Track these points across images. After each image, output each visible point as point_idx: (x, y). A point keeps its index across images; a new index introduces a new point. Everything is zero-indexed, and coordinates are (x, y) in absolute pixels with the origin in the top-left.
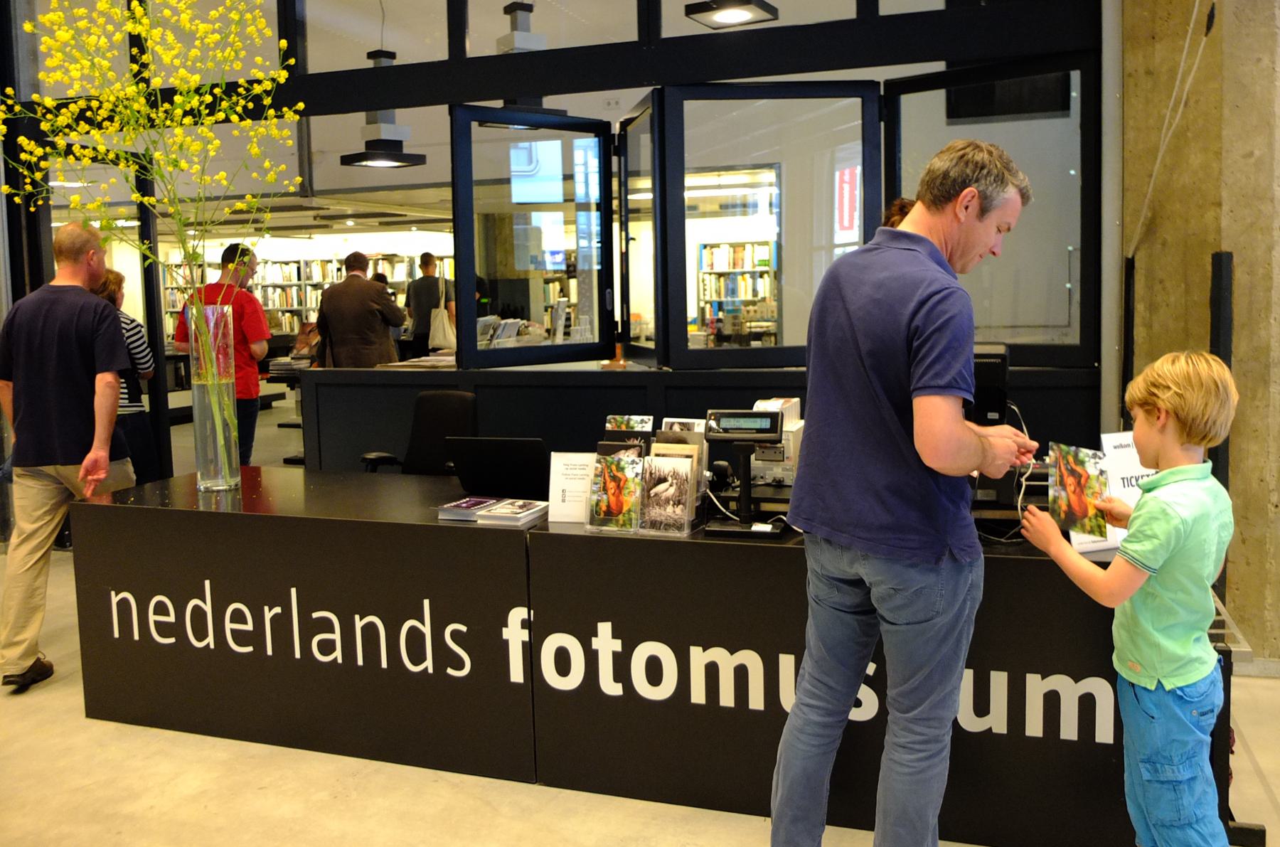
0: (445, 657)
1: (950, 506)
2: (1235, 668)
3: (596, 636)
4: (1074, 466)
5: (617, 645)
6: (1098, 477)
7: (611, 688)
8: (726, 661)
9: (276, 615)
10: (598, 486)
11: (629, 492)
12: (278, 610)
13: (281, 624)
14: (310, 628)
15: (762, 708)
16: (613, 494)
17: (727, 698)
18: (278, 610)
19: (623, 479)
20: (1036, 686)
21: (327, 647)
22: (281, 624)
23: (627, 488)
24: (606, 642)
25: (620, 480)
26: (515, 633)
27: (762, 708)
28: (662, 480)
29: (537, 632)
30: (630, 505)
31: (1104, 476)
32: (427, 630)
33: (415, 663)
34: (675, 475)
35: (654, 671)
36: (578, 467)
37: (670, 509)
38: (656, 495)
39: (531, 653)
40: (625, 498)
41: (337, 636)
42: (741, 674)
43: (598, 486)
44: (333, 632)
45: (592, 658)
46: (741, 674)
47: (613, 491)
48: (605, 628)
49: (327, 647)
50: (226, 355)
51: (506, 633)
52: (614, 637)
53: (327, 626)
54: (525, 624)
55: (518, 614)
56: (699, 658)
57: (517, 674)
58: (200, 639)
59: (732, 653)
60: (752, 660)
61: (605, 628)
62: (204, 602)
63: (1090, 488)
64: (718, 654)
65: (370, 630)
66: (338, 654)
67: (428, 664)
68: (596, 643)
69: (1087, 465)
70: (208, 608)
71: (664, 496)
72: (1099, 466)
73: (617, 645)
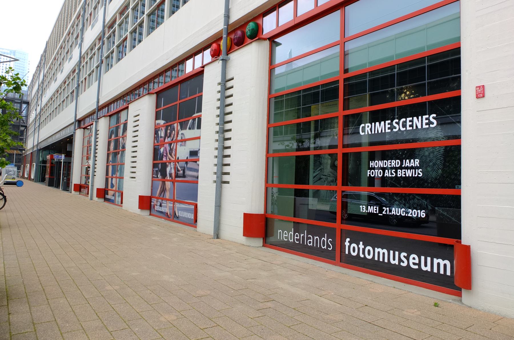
0: (328, 246)
1: (281, 147)
2: (172, 207)
3: (360, 244)
7: (362, 256)
8: (442, 262)
9: (303, 236)
12: (303, 235)
13: (303, 237)
14: (308, 238)
15: (450, 275)
17: (442, 272)
18: (303, 235)
20: (436, 261)
22: (303, 237)
24: (361, 246)
26: (347, 244)
27: (450, 275)
28: (11, 171)
29: (351, 242)
32: (326, 240)
33: (323, 247)
34: (13, 171)
36: (91, 162)
37: (12, 176)
38: (10, 174)
41: (312, 240)
42: (445, 266)
44: (311, 239)
46: (445, 266)
48: (361, 243)
50: (83, 9)
51: (346, 244)
52: (363, 245)
53: (310, 238)
54: (349, 242)
55: (348, 240)
56: (377, 250)
57: (347, 253)
58: (323, 247)
59: (443, 261)
60: (385, 251)
61: (361, 243)
62: (325, 238)
64: (440, 261)
65: (317, 239)
66: (311, 244)
67: (325, 247)
68: (360, 246)
70: (293, 234)
71: (11, 174)
73: (363, 247)
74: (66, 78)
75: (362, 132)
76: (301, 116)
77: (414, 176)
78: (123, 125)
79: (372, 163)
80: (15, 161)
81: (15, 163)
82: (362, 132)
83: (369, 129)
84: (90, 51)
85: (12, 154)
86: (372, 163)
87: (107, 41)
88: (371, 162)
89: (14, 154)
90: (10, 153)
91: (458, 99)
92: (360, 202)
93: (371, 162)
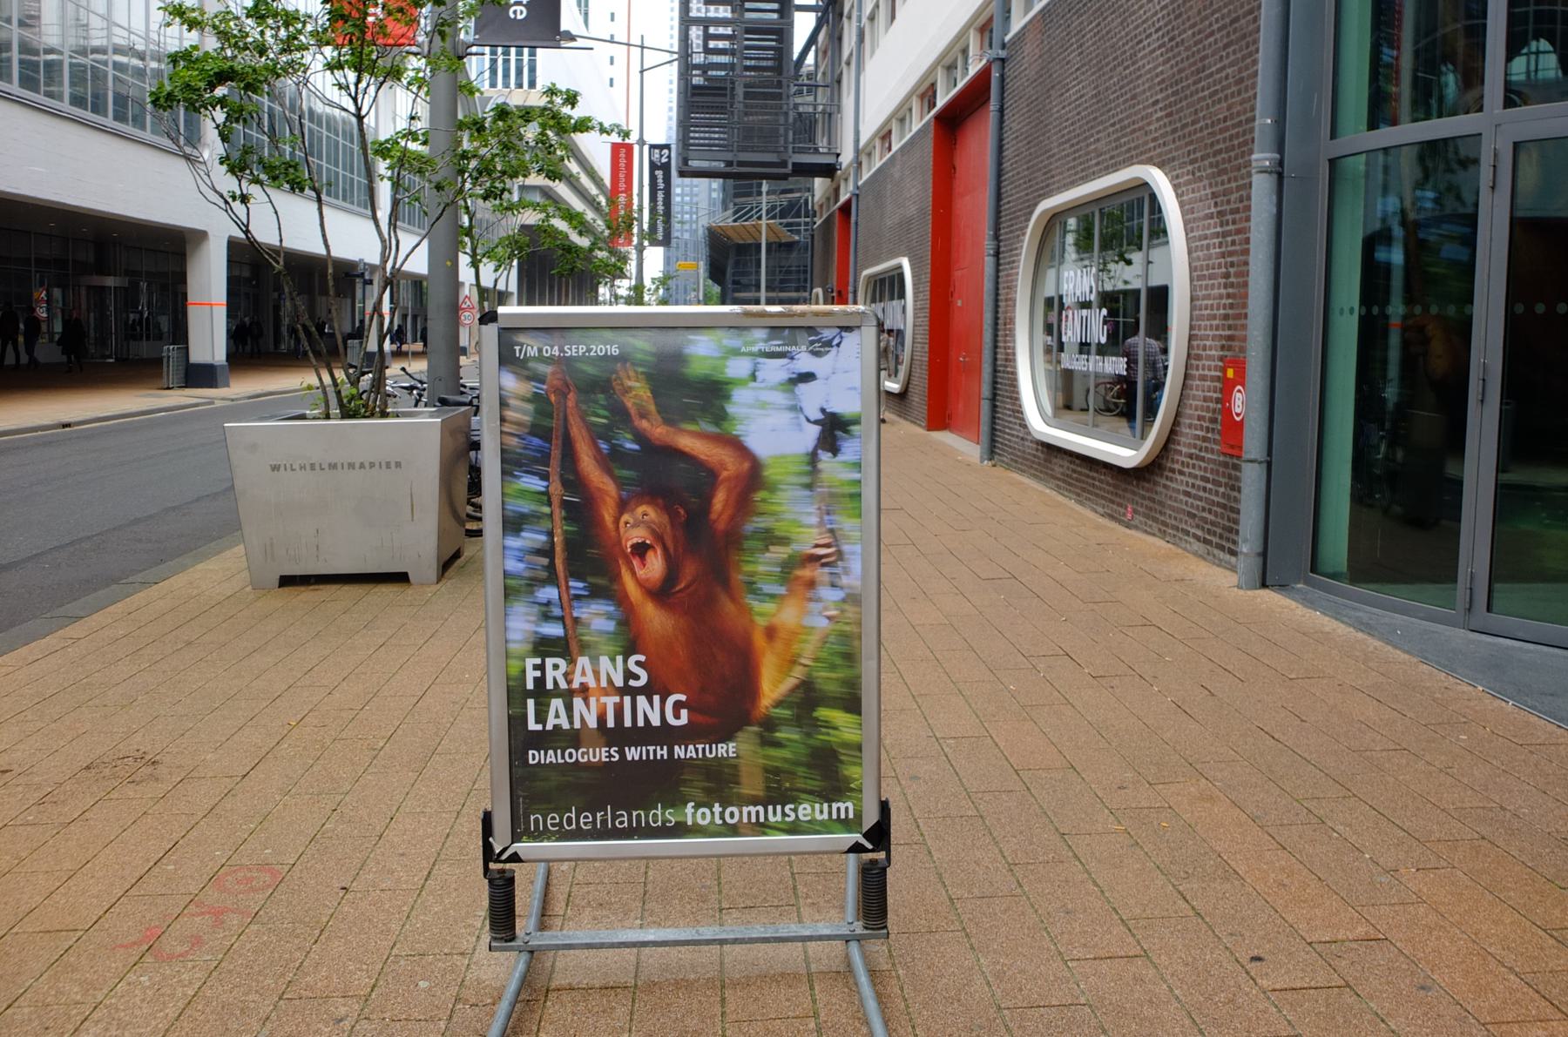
4: (658, 431)
5: (721, 809)
6: (813, 458)
10: (532, 538)
11: (788, 569)
16: (661, 593)
19: (731, 465)
21: (622, 823)
23: (770, 538)
24: (717, 808)
25: (707, 475)
30: (808, 650)
31: (850, 449)
35: (732, 815)
39: (694, 815)
40: (763, 611)
41: (626, 819)
43: (532, 538)
45: (713, 813)
46: (758, 812)
47: (655, 566)
48: (717, 805)
49: (622, 823)
60: (760, 808)
61: (717, 805)
63: (770, 538)
66: (626, 824)
69: (740, 403)
72: (813, 399)
73: (721, 809)
74: (932, 69)
75: (537, 722)
76: (92, 326)
77: (707, 746)
78: (710, 57)
79: (662, 755)
80: (767, 281)
81: (767, 291)
82: (537, 722)
83: (559, 675)
84: (945, 72)
85: (750, 245)
86: (662, 755)
87: (945, 80)
88: (665, 757)
89: (759, 246)
90: (741, 242)
91: (1485, 26)
92: (680, 830)
93: (665, 757)
